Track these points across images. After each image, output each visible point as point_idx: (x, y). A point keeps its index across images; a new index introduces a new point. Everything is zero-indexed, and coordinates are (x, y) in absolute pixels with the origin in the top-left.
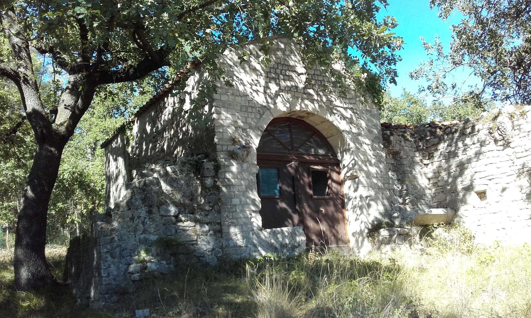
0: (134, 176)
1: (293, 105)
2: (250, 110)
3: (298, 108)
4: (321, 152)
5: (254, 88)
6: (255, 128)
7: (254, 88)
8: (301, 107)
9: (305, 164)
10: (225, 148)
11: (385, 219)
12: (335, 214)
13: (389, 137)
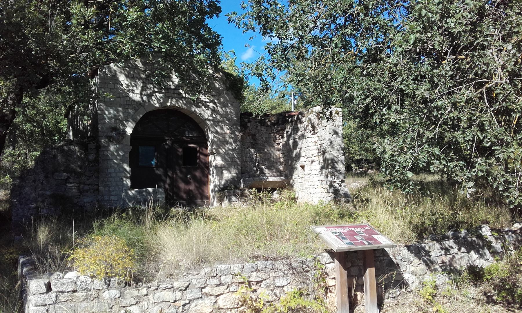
3: (169, 104)
9: (183, 144)
12: (203, 178)
13: (246, 123)
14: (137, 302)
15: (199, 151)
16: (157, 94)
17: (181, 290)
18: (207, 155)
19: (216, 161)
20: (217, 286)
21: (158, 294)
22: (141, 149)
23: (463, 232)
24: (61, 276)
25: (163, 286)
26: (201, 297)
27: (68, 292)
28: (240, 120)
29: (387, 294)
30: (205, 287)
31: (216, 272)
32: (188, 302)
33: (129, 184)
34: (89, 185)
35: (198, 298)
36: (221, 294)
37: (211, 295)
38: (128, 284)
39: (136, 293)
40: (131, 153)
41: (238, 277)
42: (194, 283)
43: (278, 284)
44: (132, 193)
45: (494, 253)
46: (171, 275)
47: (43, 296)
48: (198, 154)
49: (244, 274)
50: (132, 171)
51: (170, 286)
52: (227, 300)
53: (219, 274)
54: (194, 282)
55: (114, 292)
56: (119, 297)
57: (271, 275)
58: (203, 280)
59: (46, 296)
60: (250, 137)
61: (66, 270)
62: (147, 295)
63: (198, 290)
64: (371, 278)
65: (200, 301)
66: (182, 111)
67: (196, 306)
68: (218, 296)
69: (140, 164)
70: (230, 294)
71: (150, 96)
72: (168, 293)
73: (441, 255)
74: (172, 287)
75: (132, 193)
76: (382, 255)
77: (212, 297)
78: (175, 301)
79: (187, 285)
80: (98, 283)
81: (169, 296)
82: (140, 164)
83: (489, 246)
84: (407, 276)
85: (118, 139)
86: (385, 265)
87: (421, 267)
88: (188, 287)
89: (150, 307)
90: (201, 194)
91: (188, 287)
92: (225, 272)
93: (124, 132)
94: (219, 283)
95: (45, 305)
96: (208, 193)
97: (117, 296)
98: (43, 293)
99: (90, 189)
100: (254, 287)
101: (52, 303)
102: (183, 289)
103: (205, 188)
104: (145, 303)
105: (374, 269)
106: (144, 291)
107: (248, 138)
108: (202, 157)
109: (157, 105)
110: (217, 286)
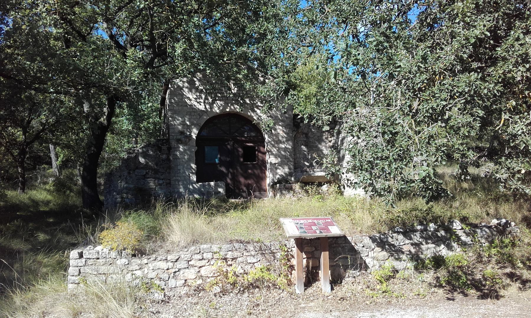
0: (336, 128)
1: (225, 107)
2: (193, 114)
3: (228, 110)
4: (253, 134)
5: (198, 100)
6: (195, 125)
7: (198, 100)
8: (230, 108)
9: (241, 143)
10: (175, 137)
11: (259, 174)
12: (261, 175)
13: (299, 123)
14: (140, 268)
15: (257, 150)
16: (218, 102)
17: (172, 262)
18: (264, 153)
19: (271, 159)
20: (200, 260)
21: (155, 263)
22: (207, 149)
23: (432, 226)
24: (92, 248)
25: (159, 258)
26: (188, 268)
27: (93, 259)
28: (293, 121)
29: (347, 274)
30: (191, 260)
31: (199, 250)
32: (177, 270)
33: (195, 179)
34: (162, 180)
35: (185, 268)
36: (203, 266)
37: (195, 266)
38: (134, 255)
39: (139, 262)
40: (197, 153)
41: (217, 254)
42: (183, 257)
43: (249, 261)
44: (197, 186)
45: (463, 244)
46: (168, 251)
47: (77, 260)
48: (257, 153)
49: (222, 252)
50: (197, 168)
51: (164, 258)
52: (208, 271)
53: (202, 252)
54: (182, 256)
55: (124, 261)
56: (128, 264)
57: (244, 254)
58: (189, 255)
59: (79, 260)
60: (304, 135)
61: (95, 244)
62: (147, 264)
63: (185, 262)
64: (324, 260)
65: (187, 270)
66: (241, 114)
67: (183, 273)
68: (200, 267)
69: (206, 162)
70: (210, 266)
71: (211, 105)
72: (162, 263)
73: (405, 244)
74: (166, 259)
75: (197, 186)
76: (344, 242)
77: (196, 268)
78: (168, 269)
79: (177, 257)
80: (113, 254)
81: (163, 265)
82: (206, 162)
83: (458, 238)
84: (368, 261)
85: (186, 141)
86: (347, 250)
87: (382, 254)
88: (178, 259)
89: (149, 272)
90: (258, 187)
91: (178, 259)
92: (206, 250)
93: (190, 136)
94: (201, 258)
95: (78, 267)
96: (265, 186)
97: (126, 263)
98: (77, 259)
99: (163, 183)
100: (229, 263)
101: (82, 265)
102: (174, 261)
103: (263, 184)
104: (146, 269)
105: (327, 253)
106: (145, 261)
107: (302, 136)
108: (260, 154)
109: (218, 111)
110: (200, 260)
